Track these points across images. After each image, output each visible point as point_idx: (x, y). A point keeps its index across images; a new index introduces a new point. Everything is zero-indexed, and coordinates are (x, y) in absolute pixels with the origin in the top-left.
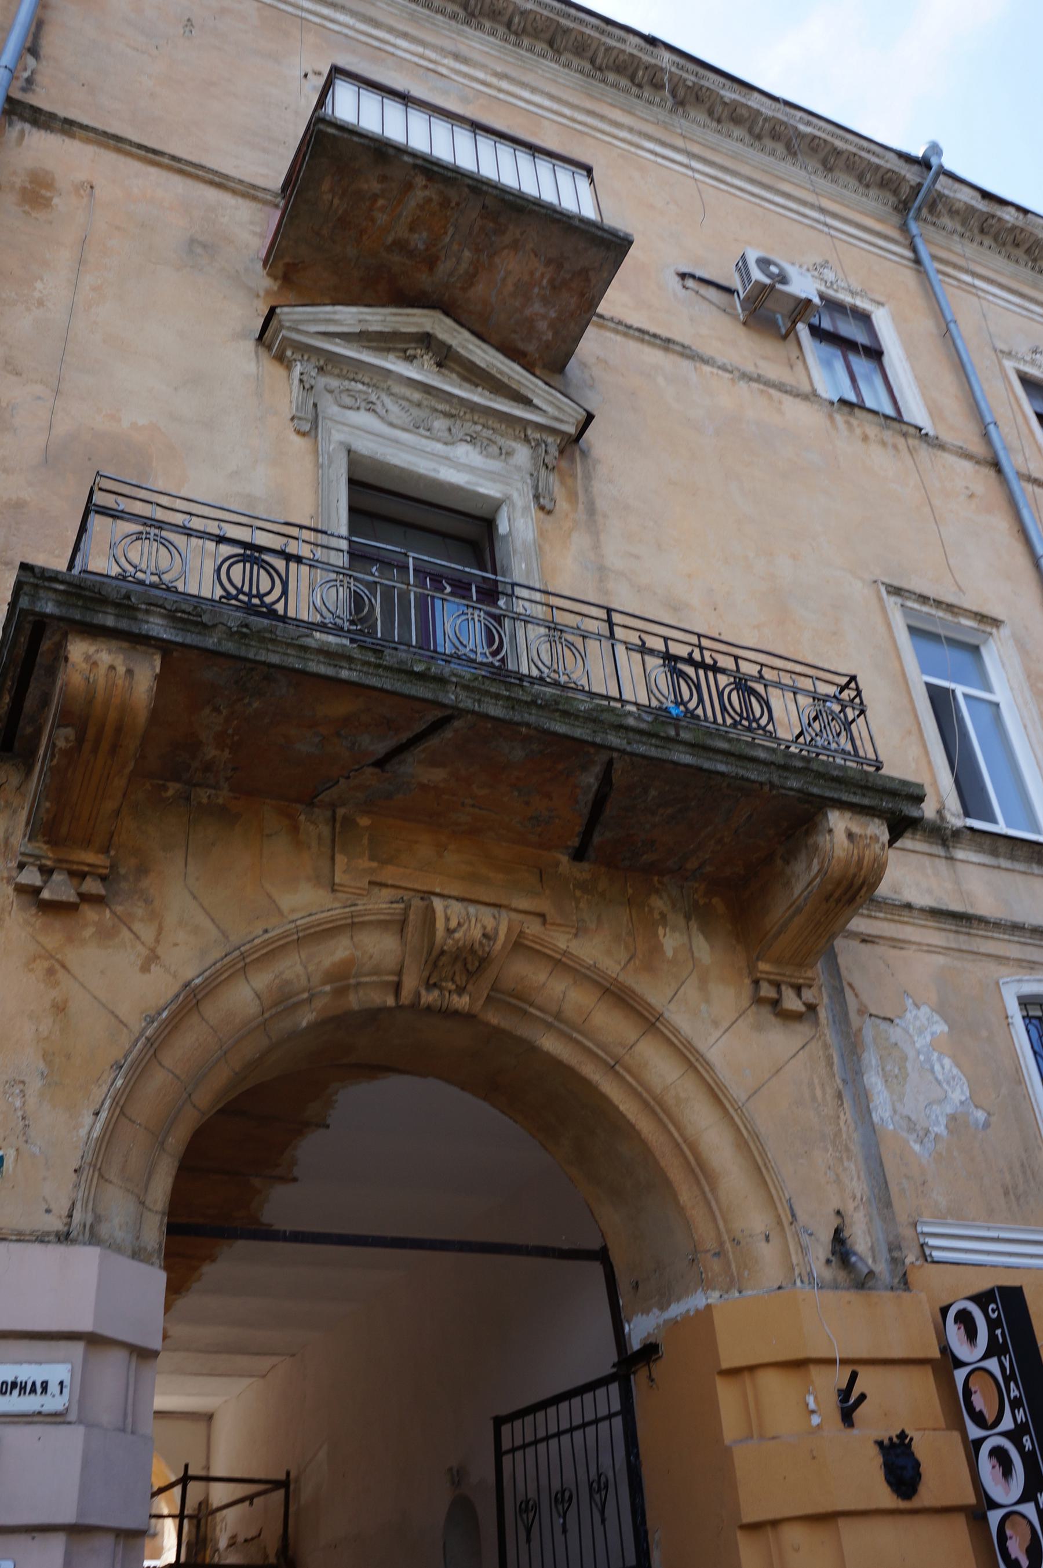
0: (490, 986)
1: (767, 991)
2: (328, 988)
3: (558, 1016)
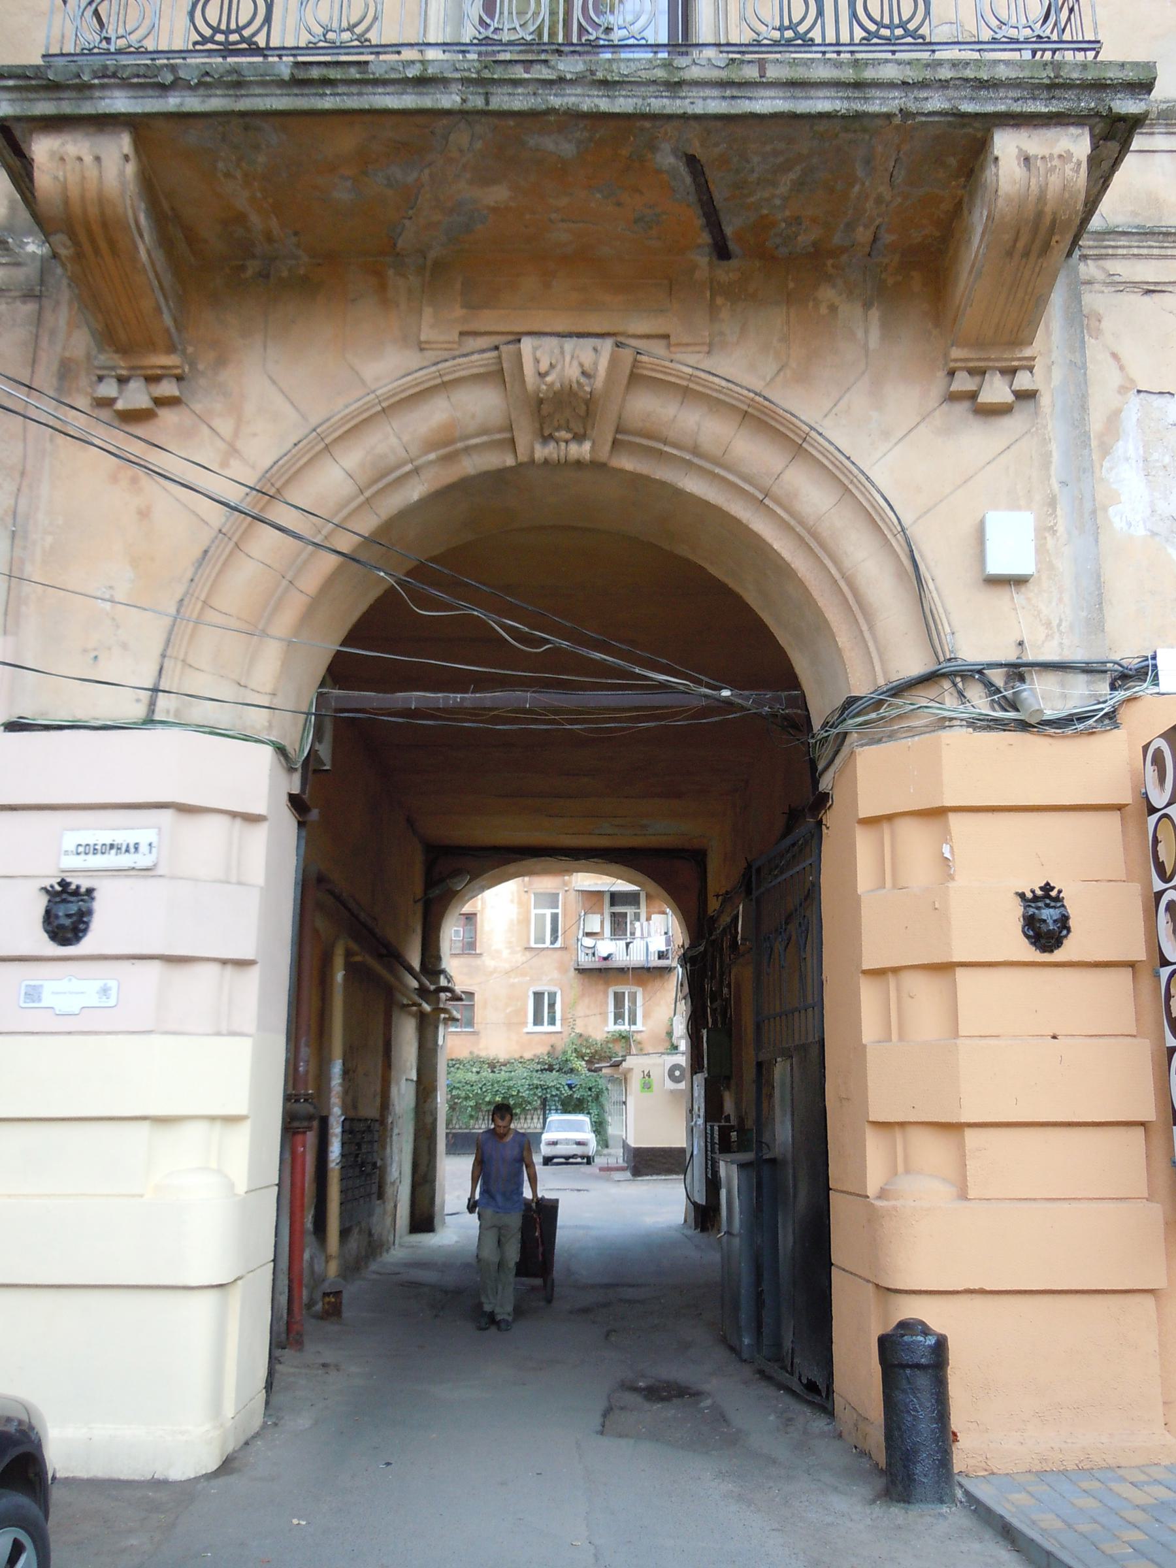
0: (613, 429)
1: (963, 383)
2: (432, 456)
3: (696, 451)
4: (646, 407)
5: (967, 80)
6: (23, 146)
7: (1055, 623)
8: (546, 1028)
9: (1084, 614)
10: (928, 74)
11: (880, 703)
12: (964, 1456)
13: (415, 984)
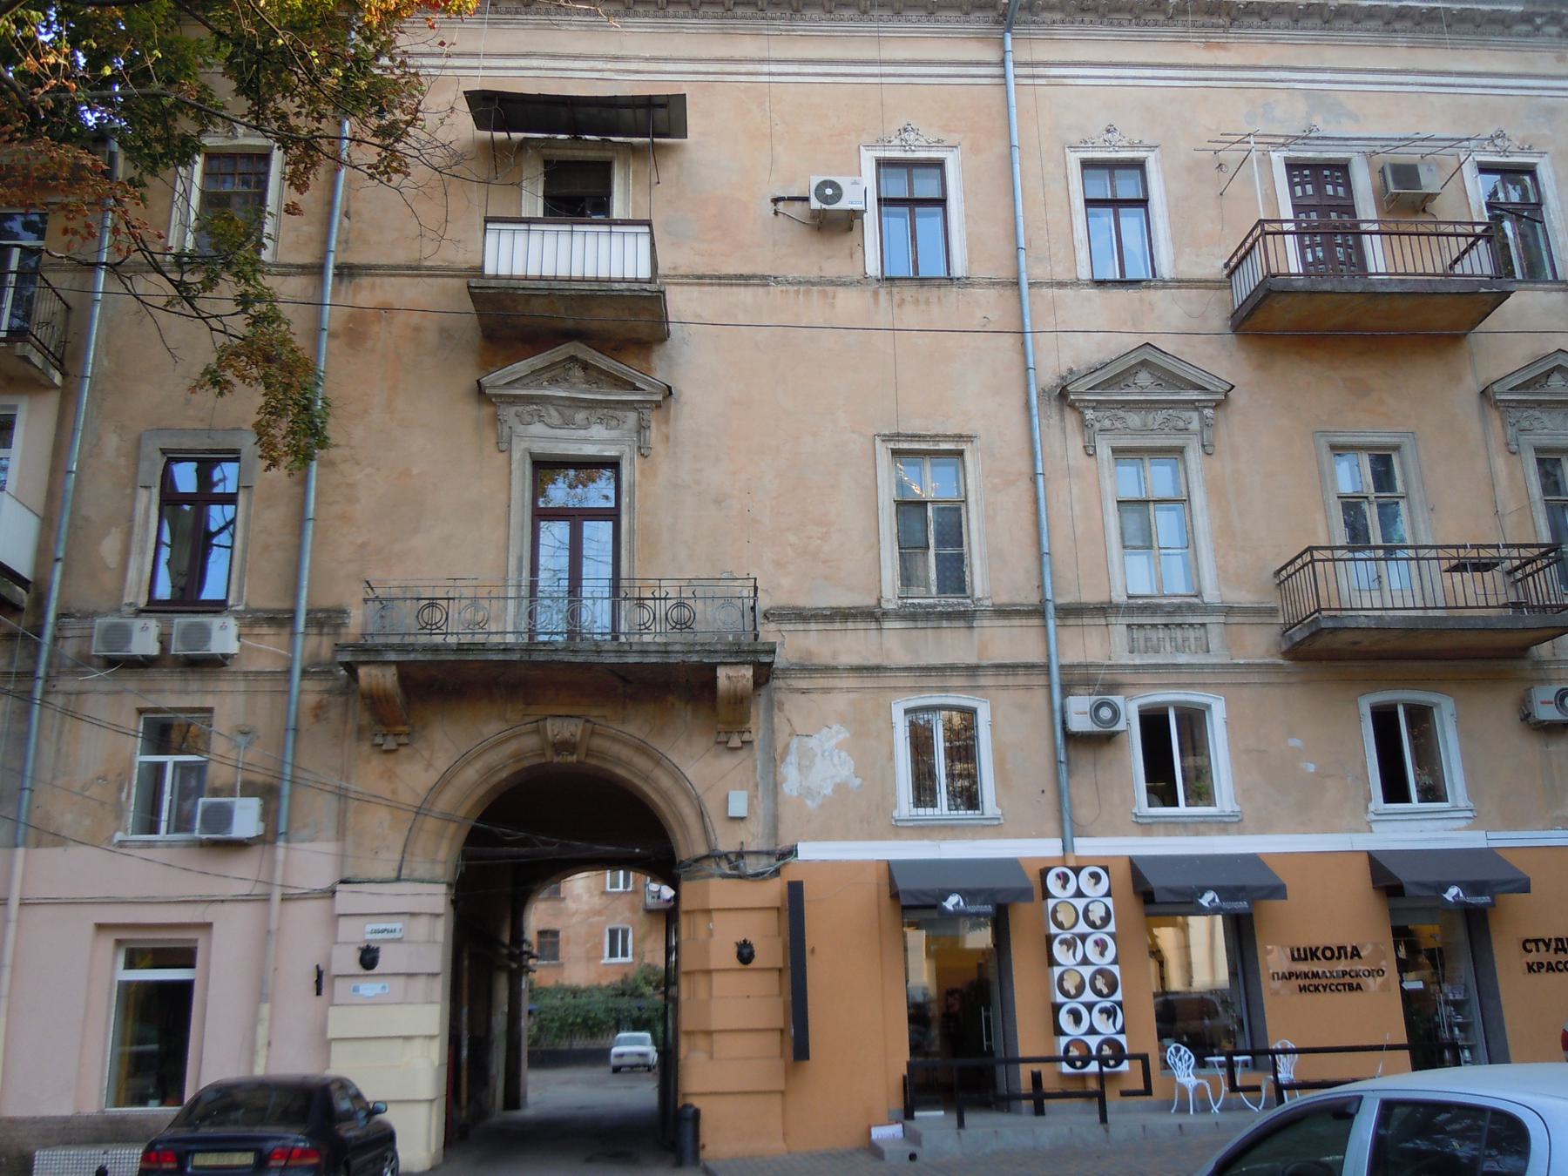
4: (597, 742)
8: (620, 959)
12: (703, 1155)
13: (505, 951)
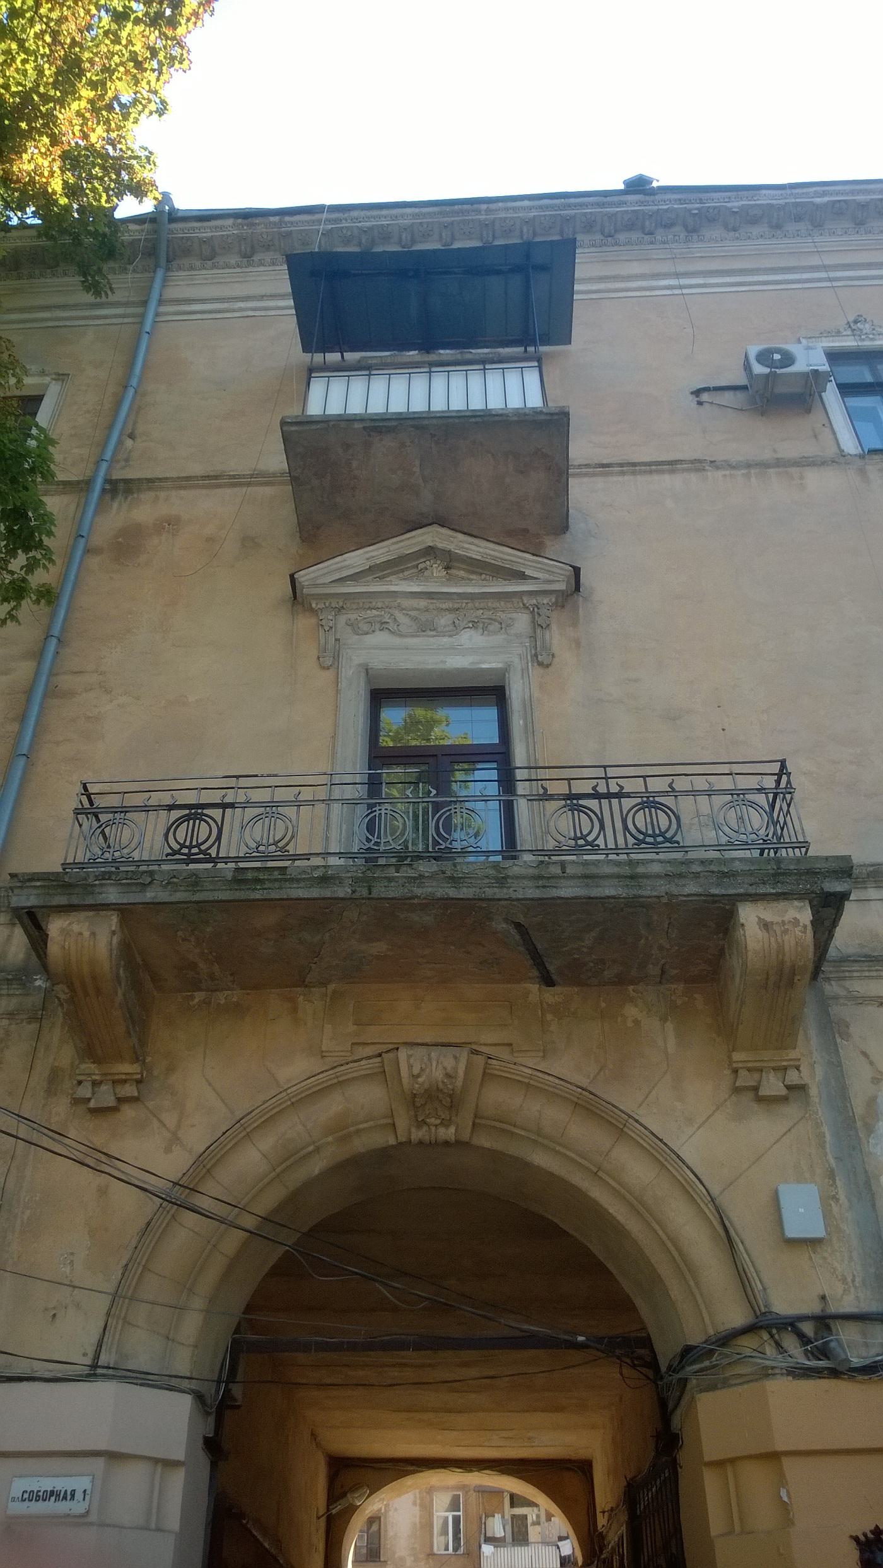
2: (330, 1139)
4: (495, 1097)
5: (713, 872)
6: (43, 925)
7: (849, 1279)
9: (872, 1270)
10: (683, 869)
11: (711, 1352)
